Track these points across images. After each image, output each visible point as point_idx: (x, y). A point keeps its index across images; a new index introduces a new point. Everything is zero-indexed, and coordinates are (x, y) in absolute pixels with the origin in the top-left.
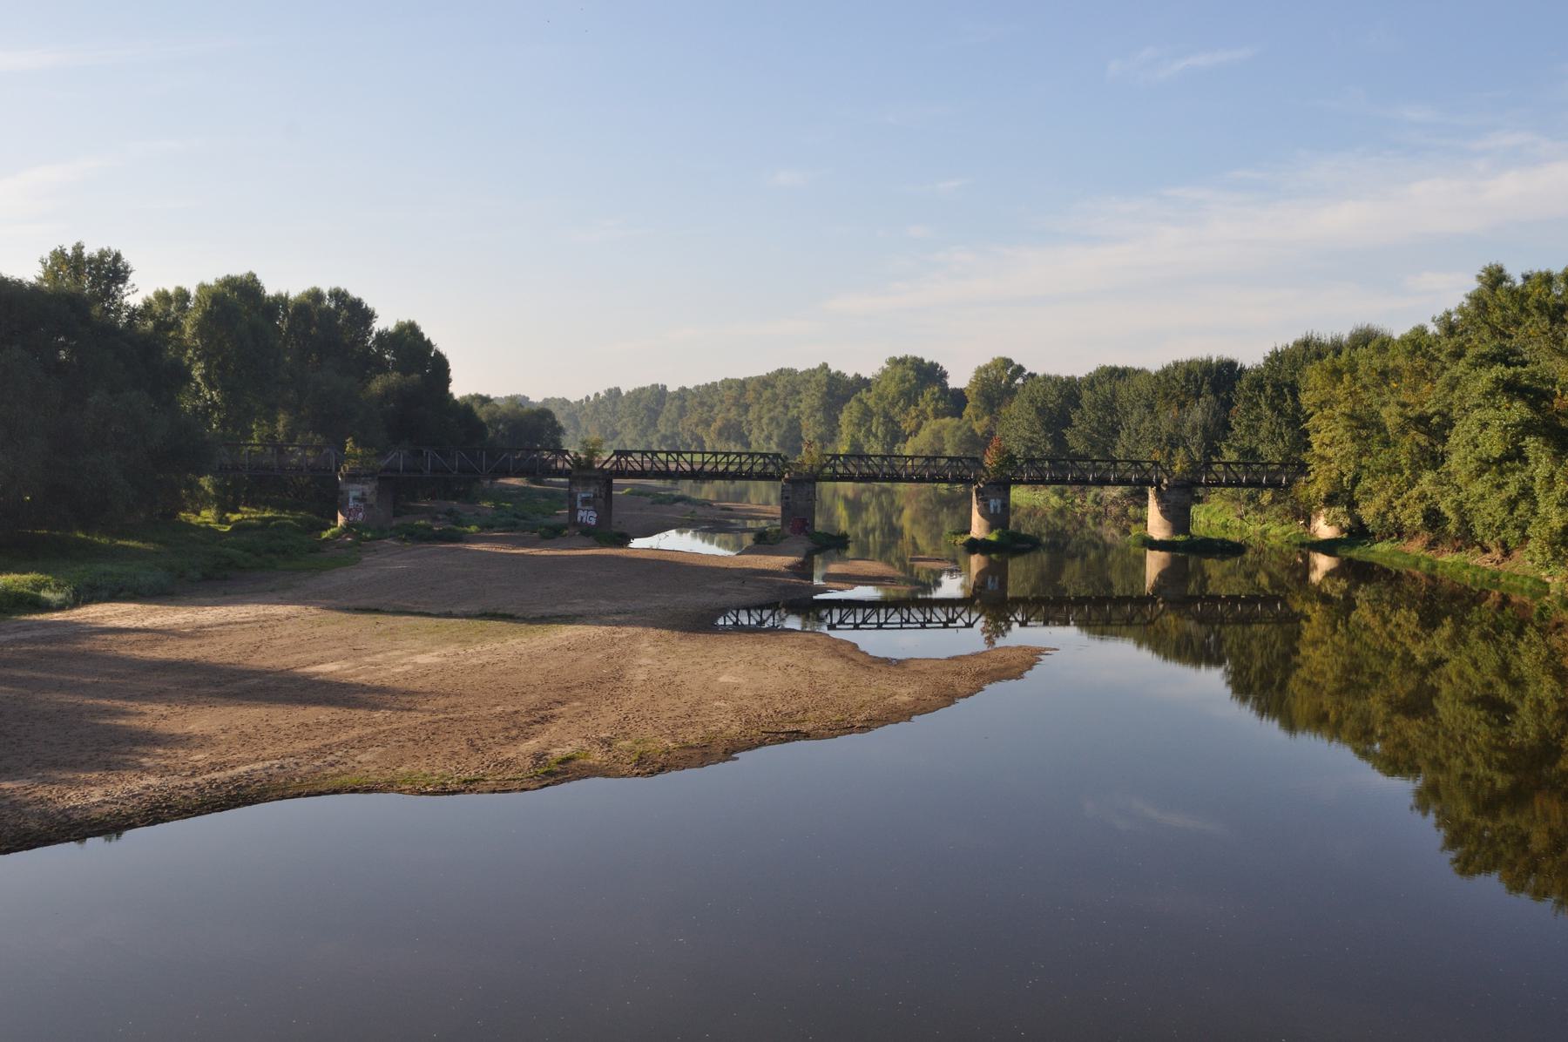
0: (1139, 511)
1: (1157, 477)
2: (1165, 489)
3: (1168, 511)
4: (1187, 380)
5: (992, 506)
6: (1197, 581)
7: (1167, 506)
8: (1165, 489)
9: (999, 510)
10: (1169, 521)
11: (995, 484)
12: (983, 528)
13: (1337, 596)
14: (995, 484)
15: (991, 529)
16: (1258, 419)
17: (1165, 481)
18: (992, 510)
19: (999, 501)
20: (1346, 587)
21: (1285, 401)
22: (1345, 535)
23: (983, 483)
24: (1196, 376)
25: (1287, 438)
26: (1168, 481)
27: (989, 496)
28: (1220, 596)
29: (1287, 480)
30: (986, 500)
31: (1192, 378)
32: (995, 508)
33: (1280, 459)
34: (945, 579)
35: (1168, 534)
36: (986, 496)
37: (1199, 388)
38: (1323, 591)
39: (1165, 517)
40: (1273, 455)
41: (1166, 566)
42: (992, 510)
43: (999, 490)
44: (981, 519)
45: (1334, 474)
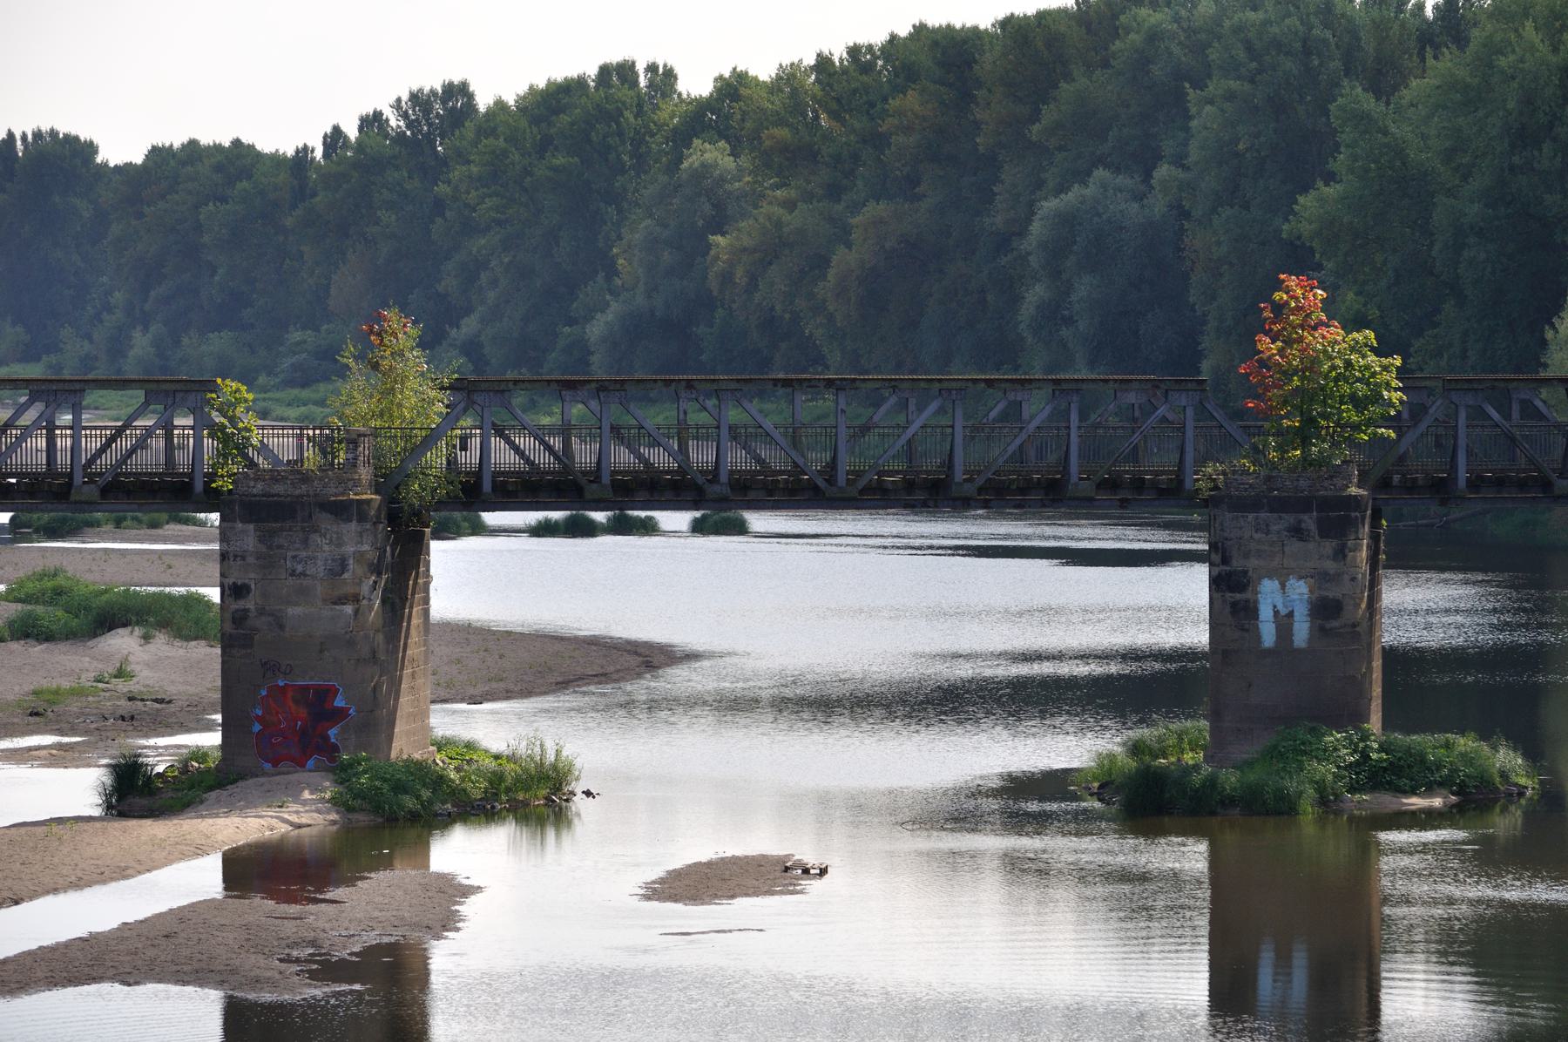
5: (1266, 613)
18: (1268, 634)
19: (1300, 590)
32: (1284, 622)
43: (1297, 532)
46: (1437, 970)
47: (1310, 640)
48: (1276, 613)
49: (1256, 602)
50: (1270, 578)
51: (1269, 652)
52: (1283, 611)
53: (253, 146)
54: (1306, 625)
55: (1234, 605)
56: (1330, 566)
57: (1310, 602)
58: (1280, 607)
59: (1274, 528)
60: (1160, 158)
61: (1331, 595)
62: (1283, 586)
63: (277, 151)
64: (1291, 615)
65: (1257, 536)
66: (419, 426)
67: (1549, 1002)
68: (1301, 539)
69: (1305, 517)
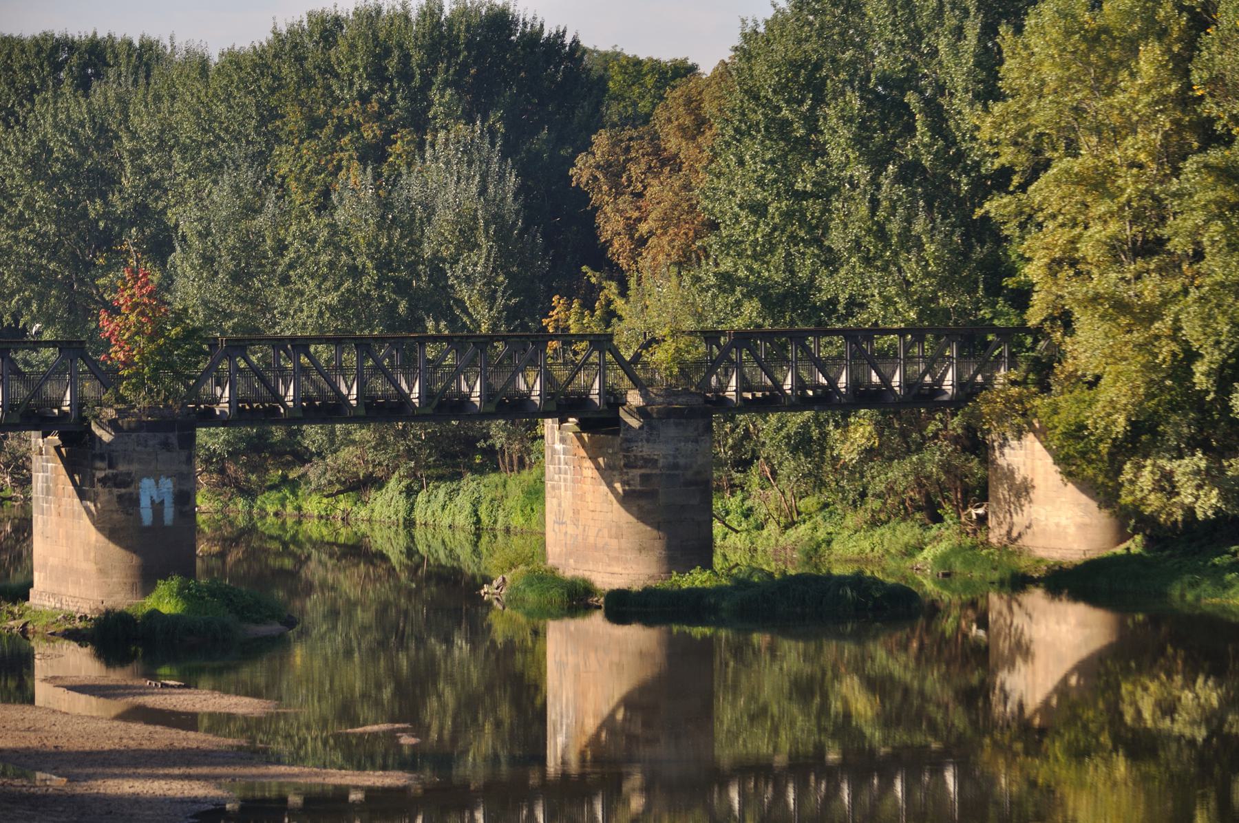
0: (241, 503)
1: (603, 383)
2: (635, 423)
3: (650, 495)
4: (378, 75)
5: (145, 502)
6: (498, 724)
7: (645, 478)
8: (635, 423)
9: (169, 514)
10: (657, 526)
11: (152, 427)
12: (116, 578)
13: (1188, 732)
14: (152, 427)
15: (146, 580)
16: (824, 192)
17: (634, 398)
18: (147, 516)
19: (167, 485)
20: (1215, 702)
21: (910, 130)
22: (1135, 545)
23: (113, 424)
24: (406, 57)
25: (930, 248)
26: (645, 395)
27: (134, 468)
28: (283, 800)
29: (959, 384)
30: (126, 484)
31: (392, 64)
32: (158, 508)
33: (912, 315)
34: (1156, 683)
35: (654, 570)
36: (122, 468)
37: (420, 97)
38: (1128, 719)
39: (642, 517)
40: (888, 302)
41: (647, 672)
42: (147, 516)
43: (166, 445)
44: (642, 526)
45: (1166, 350)
46: (446, 732)
47: (174, 519)
48: (153, 502)
49: (138, 495)
50: (148, 477)
51: (148, 529)
52: (157, 501)
53: (500, 21)
54: (172, 510)
55: (120, 497)
56: (184, 468)
57: (174, 494)
58: (155, 497)
59: (151, 443)
60: (945, 174)
61: (185, 488)
62: (157, 483)
63: (687, 59)
64: (162, 502)
65: (138, 449)
66: (418, 515)
67: (404, 722)
68: (169, 450)
69: (171, 435)
